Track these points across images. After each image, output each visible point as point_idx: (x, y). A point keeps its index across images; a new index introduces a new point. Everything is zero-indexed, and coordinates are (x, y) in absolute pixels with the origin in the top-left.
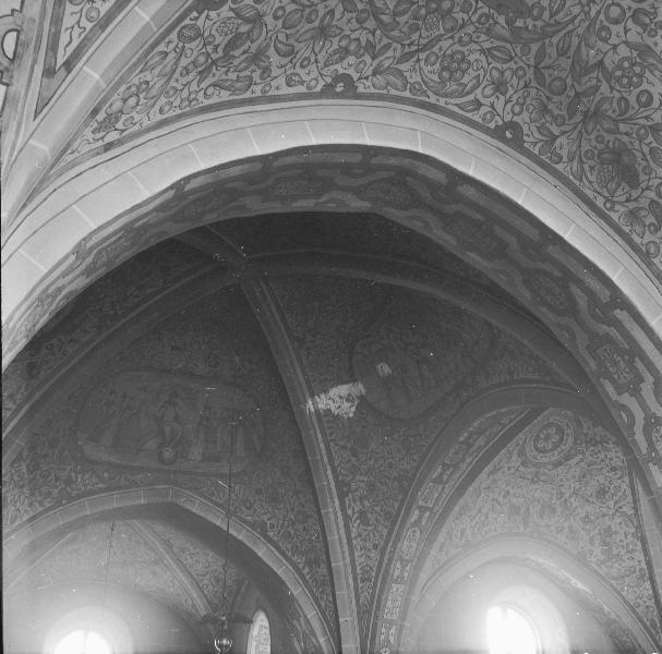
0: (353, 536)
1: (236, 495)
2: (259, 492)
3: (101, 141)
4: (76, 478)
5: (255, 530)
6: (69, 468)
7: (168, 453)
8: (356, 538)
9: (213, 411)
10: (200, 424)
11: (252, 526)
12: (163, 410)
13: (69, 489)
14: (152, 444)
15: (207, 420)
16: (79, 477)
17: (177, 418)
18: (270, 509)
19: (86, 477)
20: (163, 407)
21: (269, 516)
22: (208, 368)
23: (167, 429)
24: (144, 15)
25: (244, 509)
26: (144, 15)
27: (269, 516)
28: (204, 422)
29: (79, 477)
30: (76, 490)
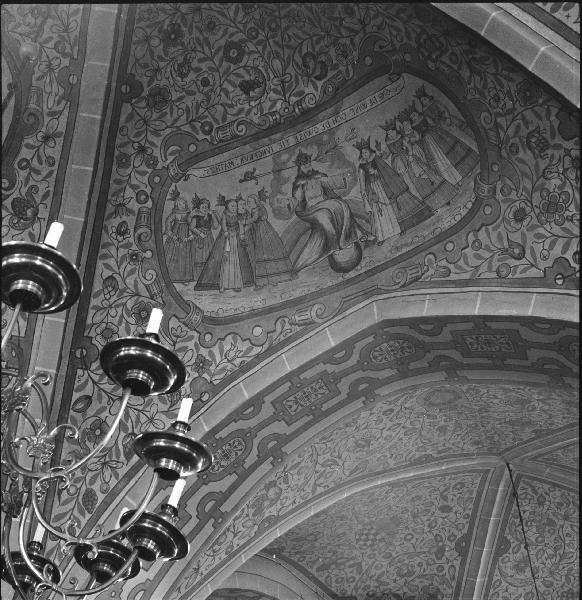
0: (134, 39)
1: (488, 249)
2: (520, 216)
3: (282, 262)
4: (211, 354)
5: (555, 285)
6: (191, 345)
7: (344, 255)
8: (138, 42)
9: (373, 146)
10: (368, 178)
11: (542, 282)
12: (299, 193)
13: (205, 375)
14: (311, 251)
15: (374, 164)
16: (216, 350)
17: (327, 192)
18: (556, 230)
19: (227, 347)
20: (295, 188)
21: (561, 243)
22: (320, 84)
23: (324, 219)
24: (246, 393)
25: (512, 262)
26: (246, 393)
27: (561, 243)
28: (372, 171)
29: (216, 350)
30: (219, 373)
